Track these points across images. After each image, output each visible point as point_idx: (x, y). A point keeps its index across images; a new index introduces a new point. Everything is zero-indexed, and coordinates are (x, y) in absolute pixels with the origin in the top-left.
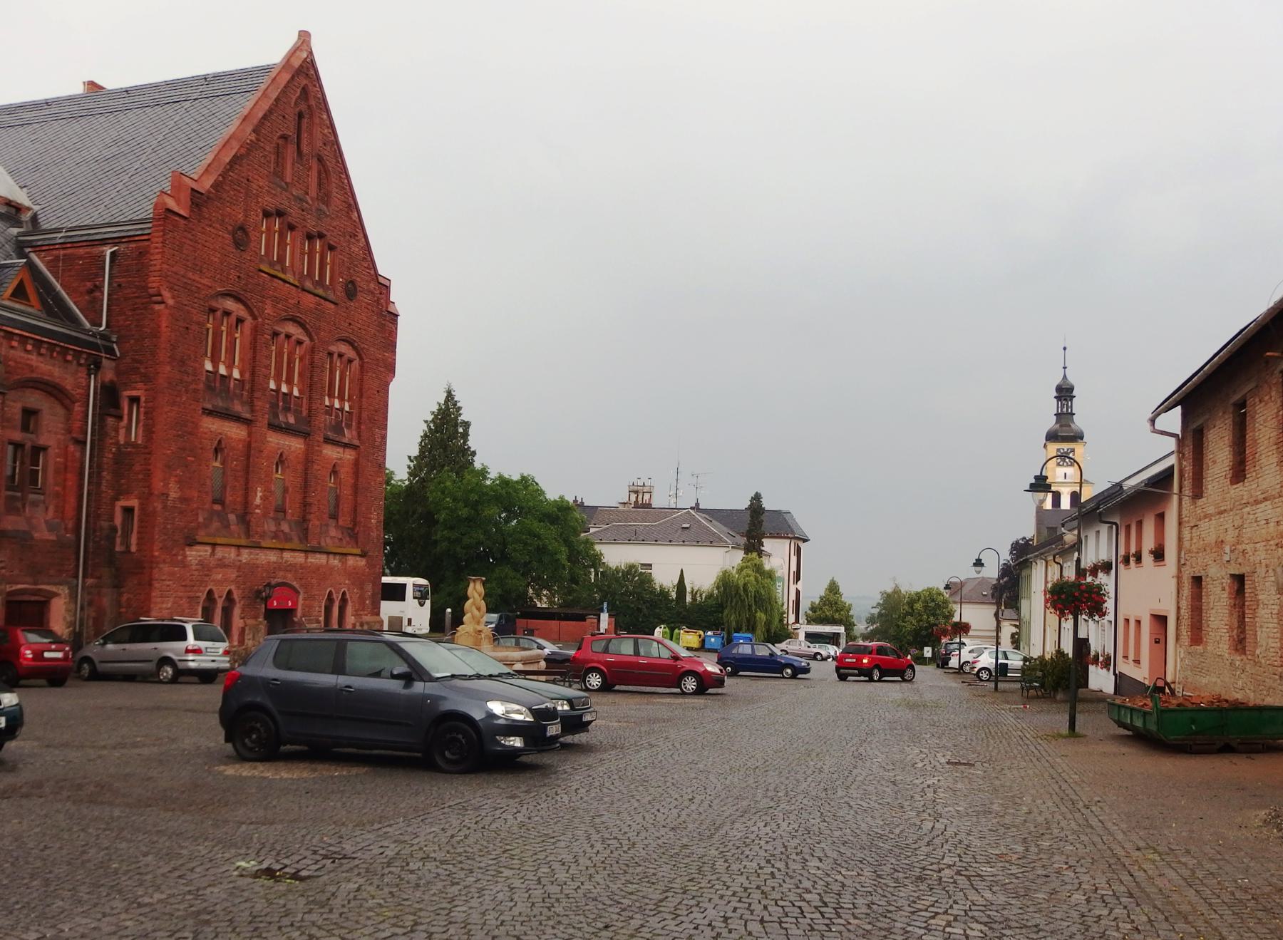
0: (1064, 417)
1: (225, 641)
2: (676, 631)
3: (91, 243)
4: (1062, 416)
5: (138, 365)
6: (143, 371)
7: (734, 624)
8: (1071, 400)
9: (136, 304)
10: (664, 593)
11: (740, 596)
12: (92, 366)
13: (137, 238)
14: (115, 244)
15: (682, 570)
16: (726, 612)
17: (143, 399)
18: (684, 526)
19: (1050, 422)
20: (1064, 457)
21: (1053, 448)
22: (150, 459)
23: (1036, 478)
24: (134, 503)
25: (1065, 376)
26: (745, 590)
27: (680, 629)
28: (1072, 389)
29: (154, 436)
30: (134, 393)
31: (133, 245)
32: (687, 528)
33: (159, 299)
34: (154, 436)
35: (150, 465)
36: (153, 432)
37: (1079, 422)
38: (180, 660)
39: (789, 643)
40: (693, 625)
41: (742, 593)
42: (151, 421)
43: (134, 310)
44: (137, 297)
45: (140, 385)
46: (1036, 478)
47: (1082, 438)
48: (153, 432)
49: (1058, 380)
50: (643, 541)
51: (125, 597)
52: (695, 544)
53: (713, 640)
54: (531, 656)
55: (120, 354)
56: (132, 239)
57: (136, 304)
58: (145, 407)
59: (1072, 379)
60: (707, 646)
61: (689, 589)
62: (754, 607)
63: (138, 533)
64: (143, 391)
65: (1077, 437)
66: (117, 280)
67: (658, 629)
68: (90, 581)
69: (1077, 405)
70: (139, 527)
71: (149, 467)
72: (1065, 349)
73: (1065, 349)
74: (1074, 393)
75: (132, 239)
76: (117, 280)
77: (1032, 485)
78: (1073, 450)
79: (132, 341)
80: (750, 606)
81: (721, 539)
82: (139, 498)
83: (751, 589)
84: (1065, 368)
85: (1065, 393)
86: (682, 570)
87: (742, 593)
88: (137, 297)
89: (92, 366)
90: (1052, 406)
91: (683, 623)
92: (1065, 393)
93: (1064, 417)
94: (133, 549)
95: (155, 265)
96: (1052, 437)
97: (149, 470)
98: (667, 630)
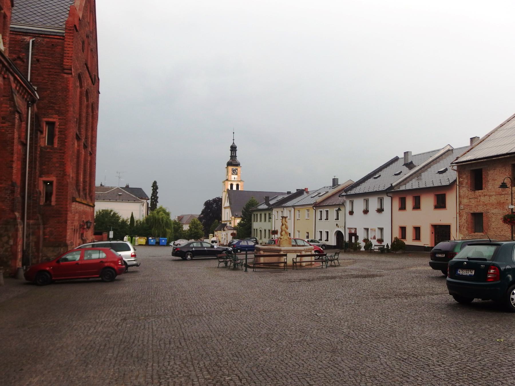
0: (233, 157)
1: (129, 249)
2: (134, 238)
3: (16, 33)
4: (234, 157)
5: (54, 105)
6: (57, 108)
7: (157, 234)
8: (236, 151)
9: (50, 72)
10: (124, 222)
11: (160, 222)
12: (30, 102)
13: (51, 37)
14: (34, 37)
15: (132, 213)
16: (153, 229)
17: (57, 124)
18: (119, 194)
19: (228, 159)
20: (234, 172)
21: (230, 168)
22: (63, 156)
23: (502, 183)
24: (54, 179)
25: (233, 143)
26: (162, 220)
27: (135, 237)
28: (236, 148)
29: (66, 144)
30: (51, 120)
31: (46, 40)
32: (121, 195)
33: (69, 71)
34: (66, 144)
35: (63, 159)
36: (66, 142)
37: (239, 159)
38: (128, 261)
39: (180, 241)
40: (140, 235)
41: (161, 222)
42: (63, 136)
43: (49, 75)
44: (51, 68)
45: (55, 116)
46: (502, 183)
47: (240, 165)
48: (66, 142)
49: (231, 144)
50: (110, 200)
51: (48, 230)
52: (127, 201)
53: (152, 241)
54: (273, 249)
55: (40, 98)
56: (46, 36)
57: (50, 72)
58: (59, 128)
59: (236, 144)
60: (150, 243)
61: (135, 221)
62: (165, 227)
63: (56, 195)
64: (58, 119)
65: (238, 165)
66: (35, 56)
67: (125, 238)
68: (31, 222)
69: (238, 153)
70: (57, 192)
71: (63, 160)
72: (234, 133)
73: (234, 133)
74: (237, 149)
75: (46, 36)
76: (35, 56)
77: (501, 186)
78: (237, 169)
79: (48, 92)
80: (164, 227)
81: (137, 199)
82: (57, 177)
83: (165, 220)
84: (233, 140)
85: (233, 149)
86: (132, 213)
87: (161, 222)
88: (51, 68)
89: (30, 102)
90: (229, 153)
91: (136, 235)
92: (233, 149)
93: (233, 157)
94: (53, 203)
95: (68, 53)
96: (229, 164)
97: (64, 162)
98: (130, 238)
